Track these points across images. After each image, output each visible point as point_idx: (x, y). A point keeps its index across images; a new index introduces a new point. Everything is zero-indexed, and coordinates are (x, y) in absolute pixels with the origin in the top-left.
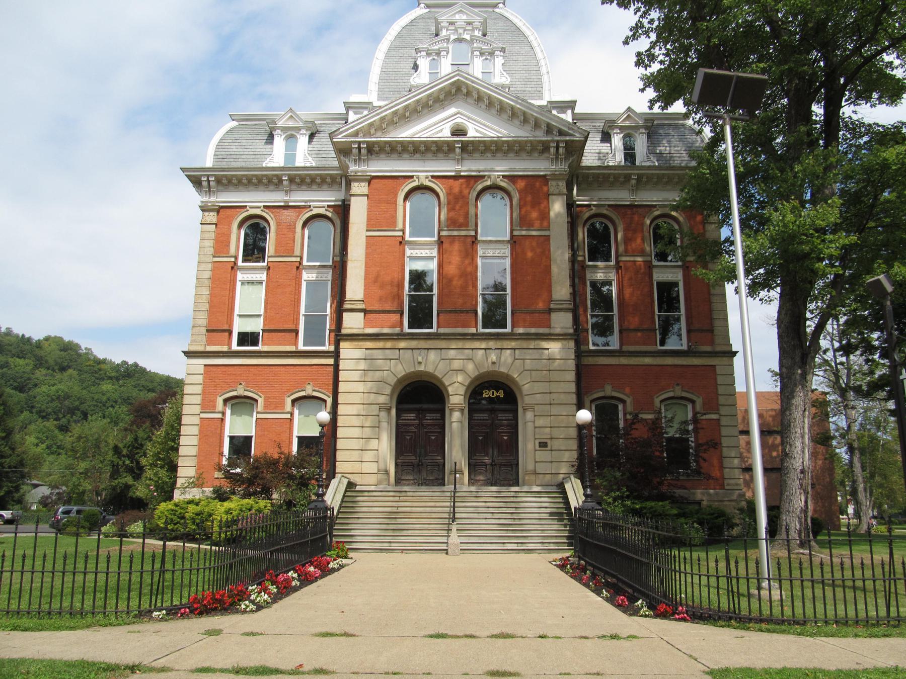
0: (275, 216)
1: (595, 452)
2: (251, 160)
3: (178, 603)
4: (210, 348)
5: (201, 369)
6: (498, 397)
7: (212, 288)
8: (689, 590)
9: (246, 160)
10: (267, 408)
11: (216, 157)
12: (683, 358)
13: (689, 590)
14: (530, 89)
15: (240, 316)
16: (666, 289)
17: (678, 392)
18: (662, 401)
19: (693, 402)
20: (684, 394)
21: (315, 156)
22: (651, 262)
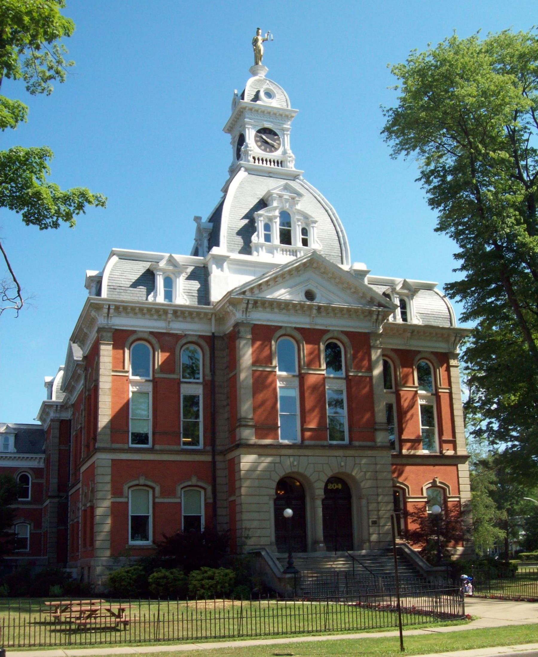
0: (159, 341)
1: (183, 528)
2: (137, 292)
3: (94, 641)
4: (115, 446)
5: (109, 463)
6: (337, 489)
7: (113, 397)
8: (208, 626)
9: (133, 292)
10: (163, 494)
11: (109, 287)
12: (143, 455)
13: (208, 626)
14: (334, 254)
15: (132, 419)
16: (192, 401)
17: (142, 481)
18: (129, 488)
19: (153, 489)
20: (200, 484)
21: (187, 294)
22: (180, 379)
